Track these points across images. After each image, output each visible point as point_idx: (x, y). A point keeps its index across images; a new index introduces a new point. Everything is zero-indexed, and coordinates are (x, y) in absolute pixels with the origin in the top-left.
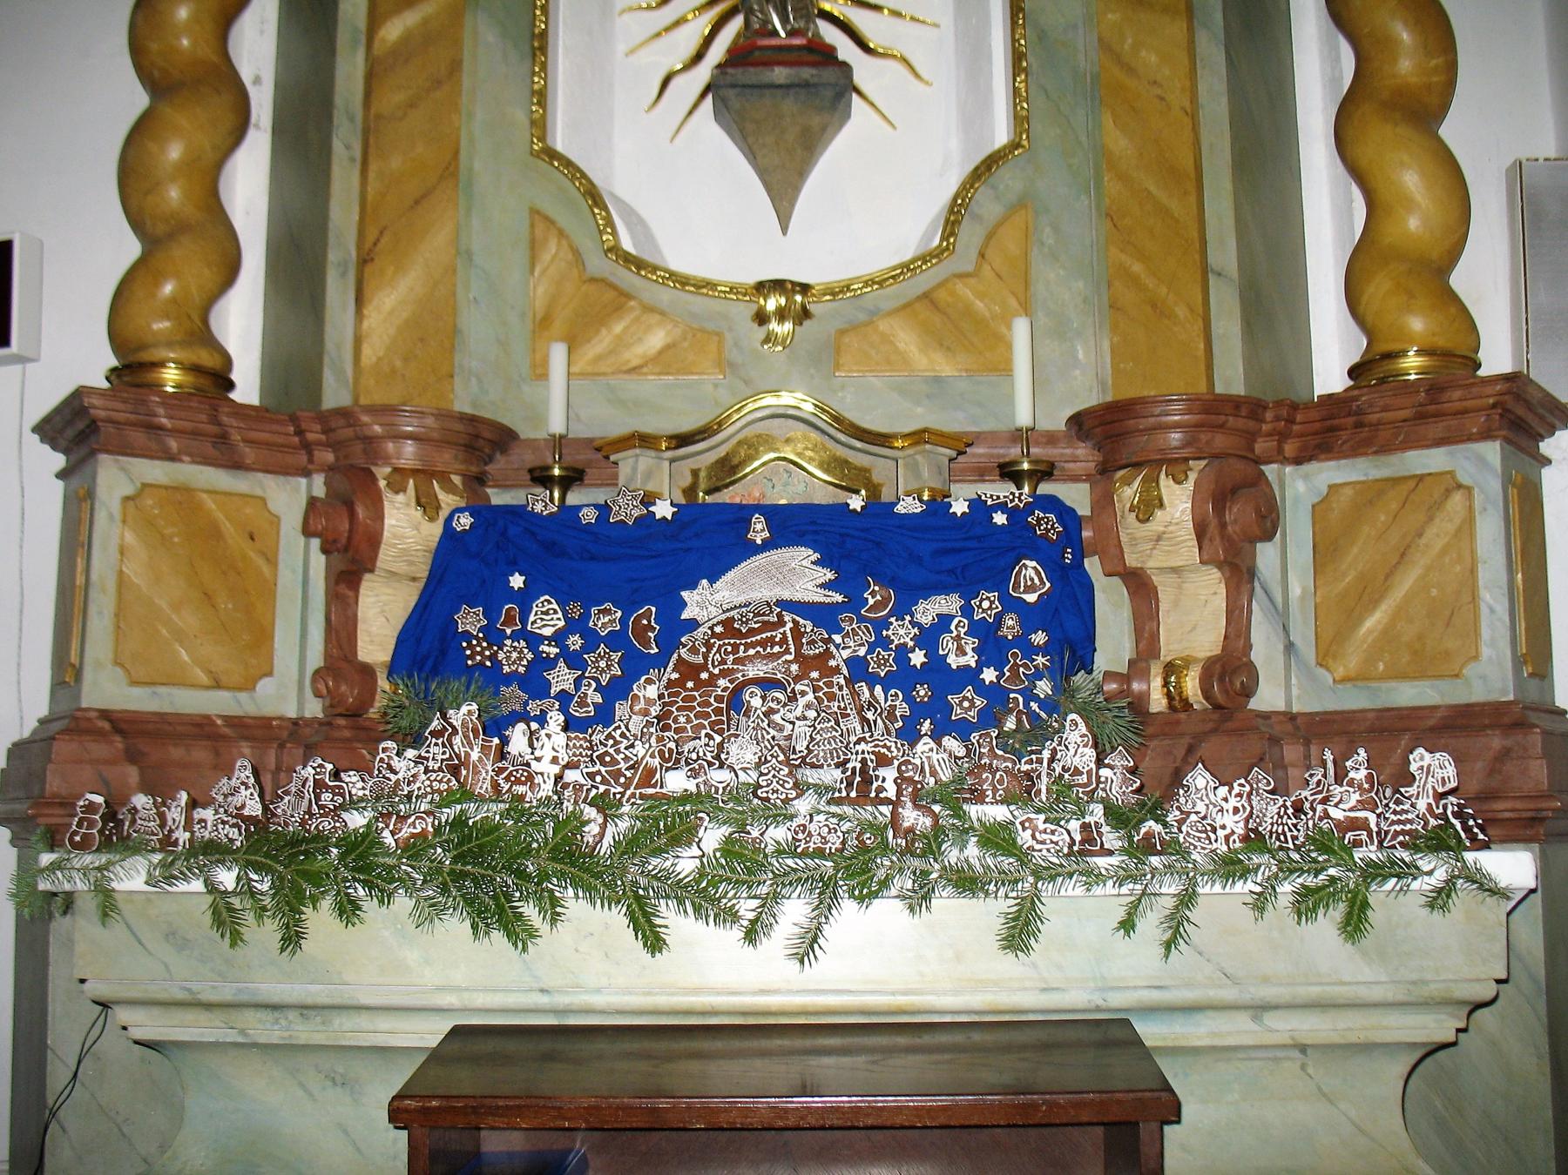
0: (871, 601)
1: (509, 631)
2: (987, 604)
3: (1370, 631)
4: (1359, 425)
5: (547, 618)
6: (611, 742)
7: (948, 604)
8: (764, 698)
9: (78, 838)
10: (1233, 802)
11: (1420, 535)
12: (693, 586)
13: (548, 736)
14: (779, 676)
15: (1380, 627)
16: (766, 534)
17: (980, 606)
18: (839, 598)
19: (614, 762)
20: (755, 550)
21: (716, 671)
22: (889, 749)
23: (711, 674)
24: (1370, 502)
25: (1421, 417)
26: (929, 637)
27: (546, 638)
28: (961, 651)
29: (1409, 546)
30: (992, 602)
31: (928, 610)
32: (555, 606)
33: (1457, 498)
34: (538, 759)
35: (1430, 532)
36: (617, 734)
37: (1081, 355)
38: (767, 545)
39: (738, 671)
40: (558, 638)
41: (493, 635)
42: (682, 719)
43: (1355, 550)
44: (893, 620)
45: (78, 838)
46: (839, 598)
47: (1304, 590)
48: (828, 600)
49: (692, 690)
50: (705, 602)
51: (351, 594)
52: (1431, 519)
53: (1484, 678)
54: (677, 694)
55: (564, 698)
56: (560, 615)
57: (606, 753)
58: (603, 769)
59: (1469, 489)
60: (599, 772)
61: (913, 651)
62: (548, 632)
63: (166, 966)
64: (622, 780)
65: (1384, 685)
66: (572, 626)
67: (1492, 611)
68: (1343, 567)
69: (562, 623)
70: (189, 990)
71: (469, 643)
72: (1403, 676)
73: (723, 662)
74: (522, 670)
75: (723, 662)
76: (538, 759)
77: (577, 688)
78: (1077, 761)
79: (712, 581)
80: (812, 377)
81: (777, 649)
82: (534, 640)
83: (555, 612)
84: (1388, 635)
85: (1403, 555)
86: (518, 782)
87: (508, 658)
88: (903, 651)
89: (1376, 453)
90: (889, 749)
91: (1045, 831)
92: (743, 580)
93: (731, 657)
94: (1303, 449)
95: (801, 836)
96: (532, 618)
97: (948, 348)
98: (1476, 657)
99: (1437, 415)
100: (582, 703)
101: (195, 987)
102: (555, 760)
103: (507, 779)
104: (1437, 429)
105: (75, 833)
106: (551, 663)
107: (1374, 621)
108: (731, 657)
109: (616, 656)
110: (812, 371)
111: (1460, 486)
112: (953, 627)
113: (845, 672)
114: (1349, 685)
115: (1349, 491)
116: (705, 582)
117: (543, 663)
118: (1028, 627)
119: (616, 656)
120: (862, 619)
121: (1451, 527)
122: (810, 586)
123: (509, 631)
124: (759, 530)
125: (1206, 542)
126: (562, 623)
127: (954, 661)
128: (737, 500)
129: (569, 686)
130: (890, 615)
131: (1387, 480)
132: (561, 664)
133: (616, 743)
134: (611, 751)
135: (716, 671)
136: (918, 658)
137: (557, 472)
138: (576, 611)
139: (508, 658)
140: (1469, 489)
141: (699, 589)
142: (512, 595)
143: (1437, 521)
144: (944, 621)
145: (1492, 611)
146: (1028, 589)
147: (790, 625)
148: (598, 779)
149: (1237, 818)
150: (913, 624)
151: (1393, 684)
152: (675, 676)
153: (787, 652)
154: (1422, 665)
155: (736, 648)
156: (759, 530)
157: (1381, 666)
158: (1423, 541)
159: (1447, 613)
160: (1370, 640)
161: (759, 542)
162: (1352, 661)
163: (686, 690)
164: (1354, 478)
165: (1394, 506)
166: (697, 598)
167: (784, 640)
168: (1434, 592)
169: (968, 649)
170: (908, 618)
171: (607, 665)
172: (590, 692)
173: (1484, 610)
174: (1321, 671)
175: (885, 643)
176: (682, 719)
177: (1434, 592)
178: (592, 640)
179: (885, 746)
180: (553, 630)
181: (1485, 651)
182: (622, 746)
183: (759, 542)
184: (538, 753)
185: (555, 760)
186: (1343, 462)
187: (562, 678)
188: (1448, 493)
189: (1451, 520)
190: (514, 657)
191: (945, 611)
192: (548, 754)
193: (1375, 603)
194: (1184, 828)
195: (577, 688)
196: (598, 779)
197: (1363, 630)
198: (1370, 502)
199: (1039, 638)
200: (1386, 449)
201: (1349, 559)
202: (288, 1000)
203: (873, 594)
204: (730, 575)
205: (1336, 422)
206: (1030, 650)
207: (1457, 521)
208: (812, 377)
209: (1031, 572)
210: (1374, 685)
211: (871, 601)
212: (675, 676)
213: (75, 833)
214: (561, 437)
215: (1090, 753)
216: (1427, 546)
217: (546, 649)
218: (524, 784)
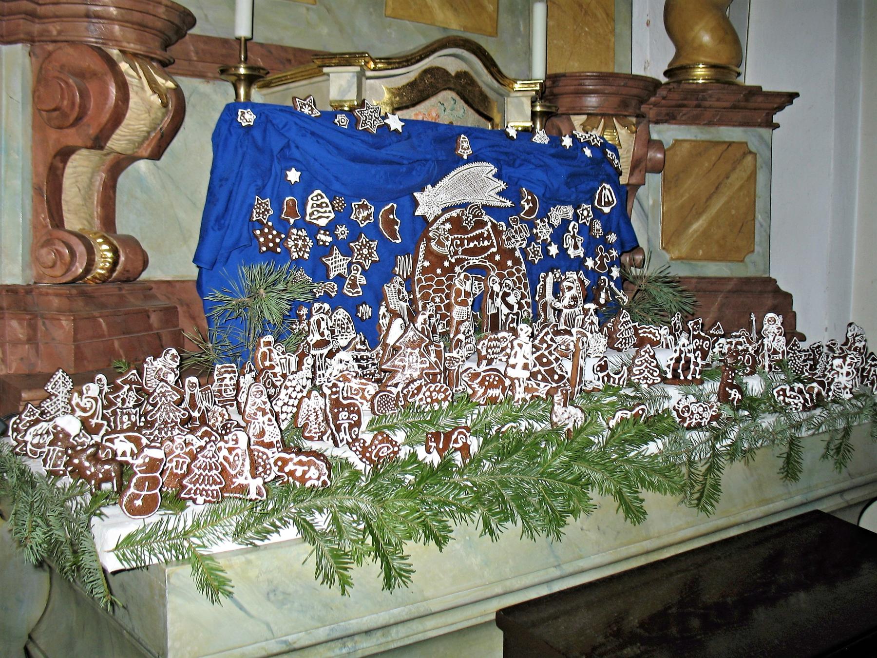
0: (527, 207)
1: (292, 221)
2: (586, 210)
3: (696, 231)
4: (698, 106)
5: (320, 209)
6: (545, 345)
7: (569, 211)
8: (501, 284)
9: (138, 503)
10: (846, 369)
11: (727, 178)
12: (422, 190)
13: (520, 346)
14: (488, 264)
15: (701, 229)
16: (470, 151)
17: (582, 214)
18: (509, 204)
19: (549, 362)
20: (459, 161)
21: (453, 261)
22: (654, 334)
23: (450, 262)
24: (700, 154)
25: (734, 107)
26: (558, 235)
27: (321, 228)
28: (576, 247)
29: (720, 184)
30: (589, 212)
31: (558, 214)
32: (326, 200)
33: (749, 158)
34: (513, 366)
35: (733, 177)
36: (548, 338)
37: (522, 28)
38: (473, 159)
39: (465, 260)
40: (330, 229)
41: (283, 227)
42: (438, 300)
43: (689, 182)
44: (538, 221)
45: (138, 503)
46: (509, 204)
47: (655, 202)
48: (502, 205)
49: (441, 275)
50: (430, 201)
51: (61, 165)
52: (734, 169)
53: (754, 263)
54: (432, 279)
55: (340, 279)
56: (330, 208)
57: (543, 355)
58: (542, 369)
59: (755, 154)
60: (539, 372)
61: (550, 244)
62: (323, 222)
63: (268, 625)
64: (556, 377)
65: (700, 263)
66: (342, 217)
67: (762, 226)
68: (681, 191)
69: (332, 216)
70: (285, 642)
71: (262, 231)
72: (713, 259)
73: (456, 253)
74: (306, 256)
75: (456, 253)
76: (513, 366)
77: (350, 272)
78: (774, 345)
79: (433, 186)
80: (371, 13)
81: (486, 243)
82: (313, 230)
83: (327, 206)
84: (705, 234)
85: (717, 188)
86: (491, 386)
87: (296, 246)
88: (545, 245)
89: (704, 125)
90: (654, 334)
91: (790, 397)
92: (454, 186)
93: (460, 249)
94: (658, 114)
95: (686, 415)
96: (309, 210)
97: (455, 10)
98: (753, 251)
99: (745, 108)
100: (354, 285)
101: (290, 638)
102: (525, 367)
103: (481, 384)
104: (739, 116)
105: (136, 497)
106: (327, 251)
107: (698, 225)
108: (460, 249)
109: (374, 244)
110: (371, 10)
111: (750, 152)
112: (570, 228)
113: (422, 247)
114: (679, 262)
115: (687, 146)
116: (429, 186)
117: (321, 252)
118: (607, 231)
119: (374, 244)
120: (522, 220)
121: (745, 175)
122: (493, 193)
123: (292, 221)
124: (465, 148)
125: (637, 172)
126: (332, 216)
127: (572, 253)
128: (420, 118)
129: (343, 271)
130: (537, 218)
131: (710, 142)
132: (336, 251)
133: (549, 346)
134: (546, 353)
135: (453, 261)
136: (553, 250)
137: (242, 71)
138: (340, 202)
139: (296, 246)
140: (755, 154)
141: (426, 193)
142: (291, 188)
143: (737, 170)
144: (565, 222)
145: (762, 226)
146: (608, 204)
147: (489, 224)
148: (540, 377)
149: (848, 379)
150: (551, 225)
151: (705, 263)
152: (426, 264)
153: (492, 246)
154: (723, 255)
155: (462, 240)
156: (465, 148)
157: (701, 252)
158: (729, 181)
159: (740, 225)
160: (695, 236)
161: (465, 157)
162: (684, 248)
163: (438, 276)
164: (688, 137)
165: (714, 158)
166: (426, 198)
167: (489, 238)
168: (733, 212)
169: (579, 245)
170: (546, 220)
171: (368, 252)
172: (358, 275)
173: (757, 225)
174: (664, 252)
175: (533, 238)
176: (438, 300)
177: (733, 212)
178: (355, 232)
179: (650, 333)
180: (327, 221)
181: (757, 248)
182: (552, 348)
183: (465, 157)
184: (512, 361)
185: (525, 367)
186: (682, 127)
187: (337, 264)
188: (745, 155)
189: (745, 171)
190: (298, 244)
191: (565, 216)
192: (520, 361)
193: (699, 215)
194: (832, 387)
195: (350, 272)
196: (540, 377)
197: (691, 231)
198: (700, 154)
199: (612, 238)
200: (710, 123)
201: (686, 186)
202: (374, 625)
203: (528, 201)
204: (445, 181)
205: (685, 102)
206: (608, 246)
207: (749, 172)
208: (371, 13)
209: (607, 192)
210: (693, 262)
211: (527, 207)
212: (426, 264)
213: (136, 497)
214: (247, 40)
215: (783, 339)
216: (731, 184)
217: (323, 237)
218: (497, 387)
